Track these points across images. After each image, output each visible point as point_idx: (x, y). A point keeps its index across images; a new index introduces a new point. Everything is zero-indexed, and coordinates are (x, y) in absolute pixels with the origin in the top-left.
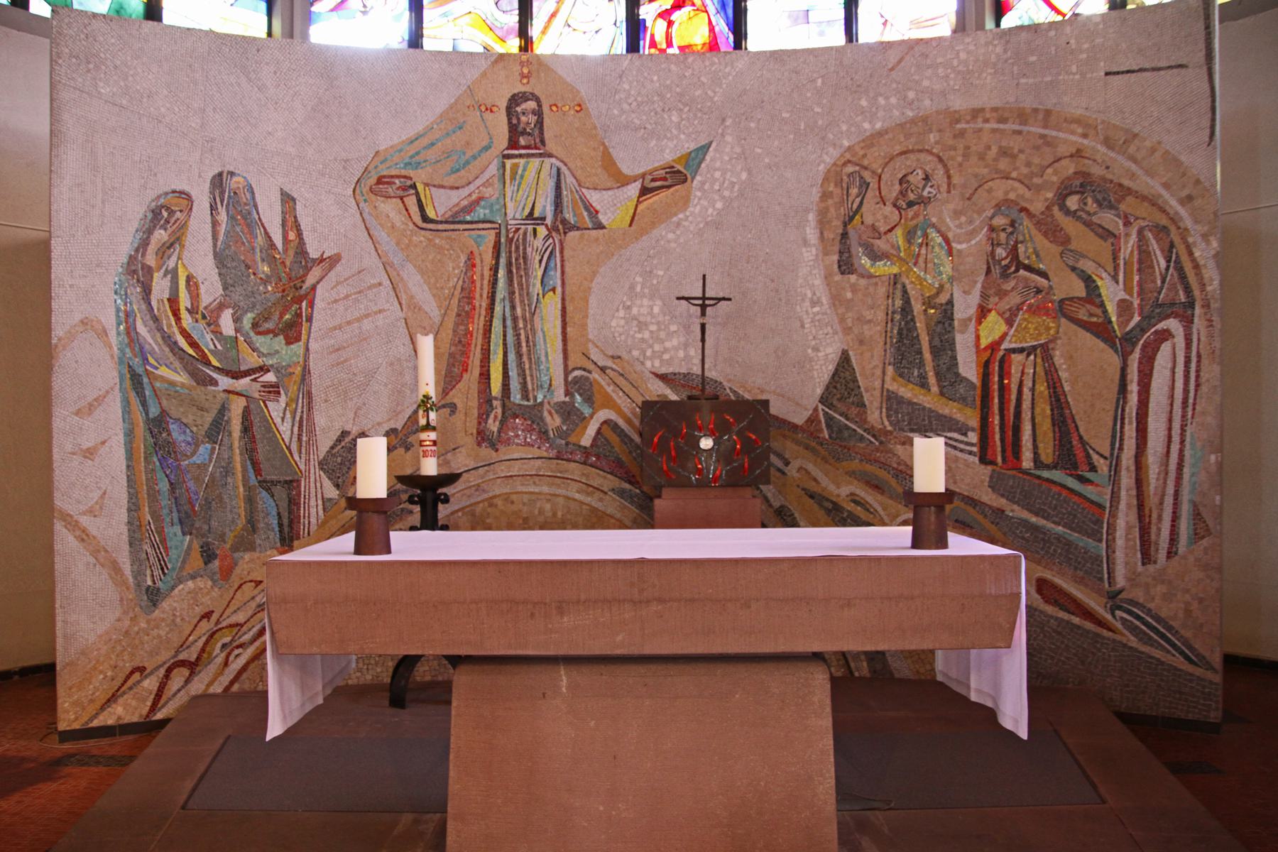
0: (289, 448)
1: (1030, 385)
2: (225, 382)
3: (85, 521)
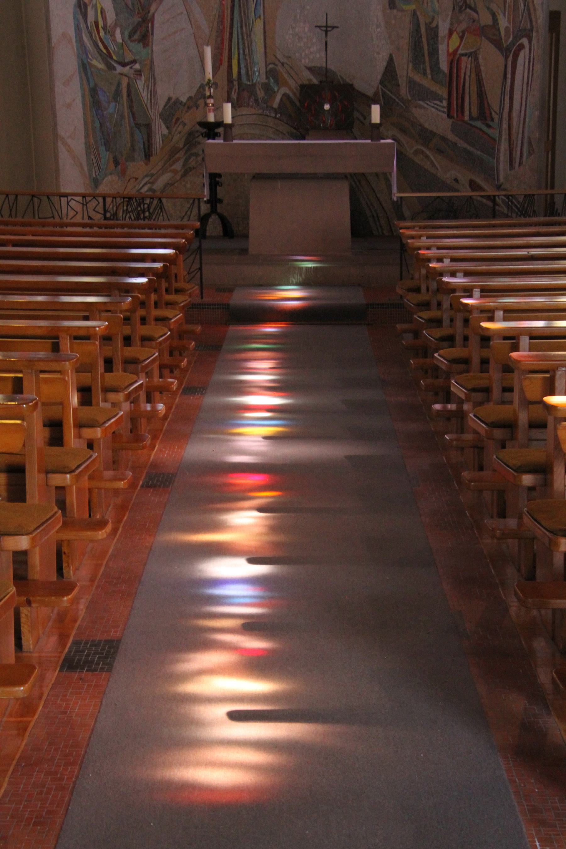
0: (146, 106)
1: (469, 74)
2: (119, 69)
3: (69, 141)
